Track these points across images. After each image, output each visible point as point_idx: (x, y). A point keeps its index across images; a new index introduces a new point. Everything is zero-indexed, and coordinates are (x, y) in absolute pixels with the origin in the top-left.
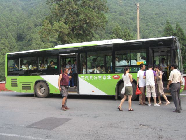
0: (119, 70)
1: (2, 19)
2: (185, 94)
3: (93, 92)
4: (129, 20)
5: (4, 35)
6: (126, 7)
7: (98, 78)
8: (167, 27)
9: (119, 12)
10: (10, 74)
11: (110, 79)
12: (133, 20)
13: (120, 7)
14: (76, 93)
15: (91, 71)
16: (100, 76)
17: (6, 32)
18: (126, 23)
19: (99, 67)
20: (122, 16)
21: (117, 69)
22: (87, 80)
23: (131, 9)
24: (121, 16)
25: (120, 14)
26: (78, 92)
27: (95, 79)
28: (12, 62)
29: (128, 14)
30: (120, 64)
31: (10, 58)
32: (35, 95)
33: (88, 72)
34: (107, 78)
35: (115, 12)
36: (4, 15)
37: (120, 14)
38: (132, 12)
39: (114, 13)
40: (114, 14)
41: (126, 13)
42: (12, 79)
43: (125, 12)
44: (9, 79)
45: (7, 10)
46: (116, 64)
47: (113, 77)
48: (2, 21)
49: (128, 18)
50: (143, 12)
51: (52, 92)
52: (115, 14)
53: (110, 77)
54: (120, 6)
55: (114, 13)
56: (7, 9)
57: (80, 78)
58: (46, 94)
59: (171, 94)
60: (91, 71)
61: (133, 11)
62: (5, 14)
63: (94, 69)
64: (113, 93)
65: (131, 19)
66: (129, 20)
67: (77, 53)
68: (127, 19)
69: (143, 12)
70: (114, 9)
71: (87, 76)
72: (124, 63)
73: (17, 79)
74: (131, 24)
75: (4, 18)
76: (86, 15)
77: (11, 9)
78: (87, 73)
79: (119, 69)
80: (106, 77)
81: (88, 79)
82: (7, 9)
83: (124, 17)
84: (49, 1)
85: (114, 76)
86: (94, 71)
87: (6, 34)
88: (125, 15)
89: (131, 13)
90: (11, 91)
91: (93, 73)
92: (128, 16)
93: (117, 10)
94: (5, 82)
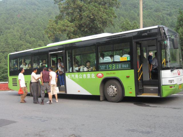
0: (103, 67)
1: (40, 23)
2: (182, 94)
3: (79, 92)
4: (165, 15)
5: (41, 37)
6: (163, 3)
7: (82, 77)
8: (180, 18)
9: (154, 9)
10: (11, 75)
11: (94, 78)
12: (170, 16)
13: (156, 3)
14: (156, 96)
15: (77, 68)
16: (84, 75)
17: (43, 35)
18: (162, 19)
19: (88, 63)
20: (158, 12)
21: (101, 66)
22: (73, 79)
23: (168, 4)
24: (157, 12)
25: (156, 11)
26: (66, 92)
27: (80, 78)
28: (13, 61)
29: (164, 10)
30: (104, 61)
31: (12, 58)
32: (106, 98)
33: (74, 71)
34: (91, 76)
35: (151, 8)
36: (42, 19)
37: (156, 11)
38: (169, 7)
39: (149, 10)
40: (150, 10)
41: (163, 9)
42: (13, 79)
43: (161, 8)
44: (11, 78)
45: (46, 14)
46: (99, 61)
47: (97, 76)
48: (40, 24)
49: (164, 13)
50: (180, 6)
51: (127, 94)
52: (151, 11)
53: (94, 75)
54: (156, 2)
55: (150, 9)
56: (47, 13)
57: (66, 77)
58: (120, 97)
59: (158, 95)
60: (77, 68)
61: (170, 6)
62: (44, 18)
63: (80, 67)
64: (97, 93)
65: (168, 14)
66: (165, 15)
67: (64, 51)
68: (163, 14)
69: (180, 6)
70: (150, 6)
71: (73, 75)
72: (108, 59)
73: (16, 79)
74: (167, 19)
75: (42, 22)
76: (90, 12)
77: (50, 13)
78: (73, 72)
79: (103, 66)
80: (90, 75)
81: (74, 78)
82: (47, 13)
83: (160, 13)
84: (67, 0)
85: (98, 74)
86: (79, 69)
87: (43, 37)
88: (162, 11)
89: (168, 8)
90: (13, 90)
91: (79, 71)
92: (164, 12)
93: (153, 7)
94: (8, 82)
